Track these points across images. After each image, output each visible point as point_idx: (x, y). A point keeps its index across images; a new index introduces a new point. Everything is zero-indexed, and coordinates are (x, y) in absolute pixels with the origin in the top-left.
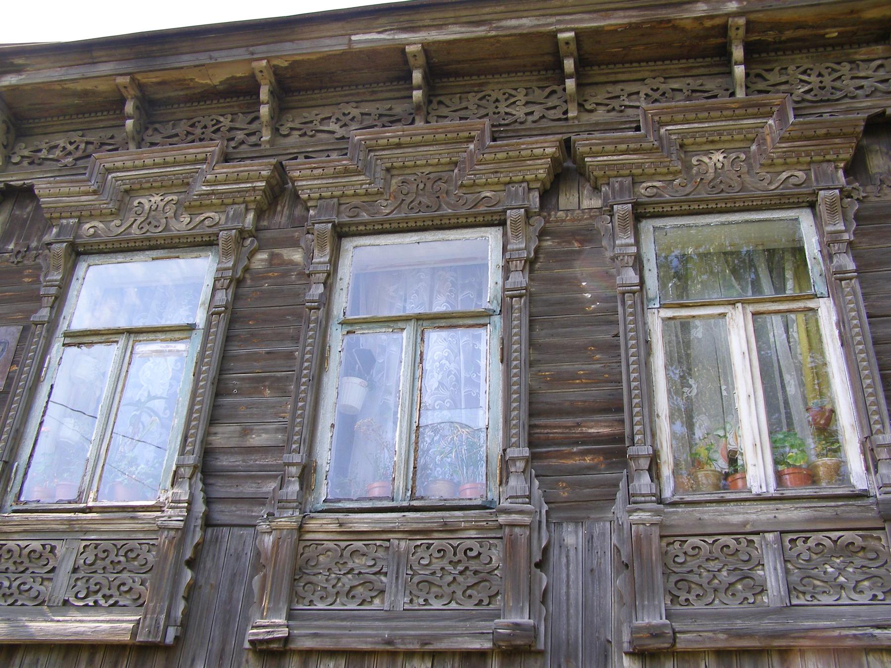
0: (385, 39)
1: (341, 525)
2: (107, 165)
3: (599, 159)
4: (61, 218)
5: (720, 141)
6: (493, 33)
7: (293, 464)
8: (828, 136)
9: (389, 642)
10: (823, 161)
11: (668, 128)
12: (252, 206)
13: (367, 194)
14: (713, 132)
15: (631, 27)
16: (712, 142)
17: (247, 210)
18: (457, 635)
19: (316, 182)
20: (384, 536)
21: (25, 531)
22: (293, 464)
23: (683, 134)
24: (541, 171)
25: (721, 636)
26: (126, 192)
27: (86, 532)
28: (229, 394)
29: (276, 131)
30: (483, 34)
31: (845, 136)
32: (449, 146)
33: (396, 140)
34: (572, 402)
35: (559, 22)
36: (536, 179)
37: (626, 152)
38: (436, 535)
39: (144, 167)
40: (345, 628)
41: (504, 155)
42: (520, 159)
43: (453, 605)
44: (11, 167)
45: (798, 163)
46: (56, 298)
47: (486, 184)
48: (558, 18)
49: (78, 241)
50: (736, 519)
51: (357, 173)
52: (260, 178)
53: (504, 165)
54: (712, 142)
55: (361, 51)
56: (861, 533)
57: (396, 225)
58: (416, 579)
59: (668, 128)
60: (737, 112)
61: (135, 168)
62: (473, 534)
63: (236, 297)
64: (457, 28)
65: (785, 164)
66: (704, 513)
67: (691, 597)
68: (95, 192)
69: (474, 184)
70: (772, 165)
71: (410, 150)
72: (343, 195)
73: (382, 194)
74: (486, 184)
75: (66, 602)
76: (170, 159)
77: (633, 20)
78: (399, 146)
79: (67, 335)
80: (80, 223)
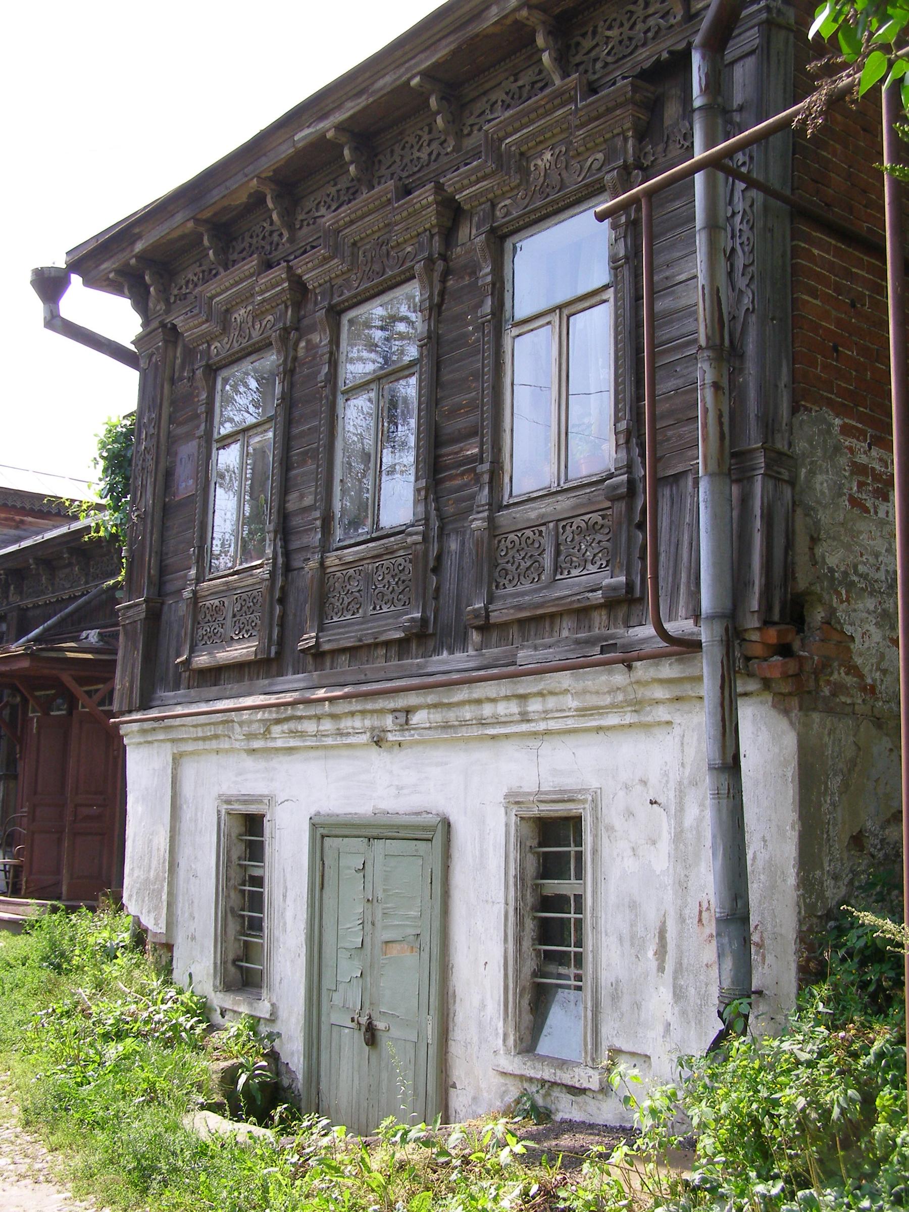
0: (311, 133)
1: (340, 559)
2: (209, 295)
3: (464, 193)
4: (198, 345)
5: (545, 140)
6: (371, 100)
7: (316, 519)
8: (609, 111)
9: (360, 640)
10: (614, 137)
11: (507, 141)
12: (289, 303)
13: (343, 273)
14: (542, 132)
15: (454, 53)
16: (541, 142)
17: (287, 307)
18: (389, 630)
19: (313, 273)
20: (361, 563)
21: (212, 594)
22: (316, 519)
23: (517, 143)
24: (430, 218)
25: (512, 611)
26: (227, 311)
27: (235, 589)
28: (294, 468)
29: (291, 228)
30: (364, 103)
31: (618, 106)
32: (381, 211)
33: (347, 219)
34: (459, 430)
35: (408, 70)
36: (433, 226)
37: (478, 181)
38: (385, 557)
39: (227, 289)
40: (339, 634)
41: (405, 214)
42: (416, 213)
43: (393, 608)
44: (173, 306)
45: (597, 145)
46: (207, 413)
47: (405, 241)
48: (407, 65)
49: (211, 362)
50: (533, 515)
51: (332, 258)
52: (283, 281)
53: (410, 221)
54: (541, 142)
55: (304, 148)
56: (600, 513)
57: (376, 290)
58: (377, 591)
59: (507, 141)
60: (547, 107)
61: (224, 291)
62: (401, 553)
63: (292, 385)
64: (349, 104)
65: (587, 149)
66: (516, 512)
67: (506, 582)
68: (207, 321)
69: (398, 244)
70: (579, 154)
71: (360, 223)
72: (331, 279)
73: (352, 270)
74: (405, 241)
75: (232, 638)
76: (237, 279)
77: (452, 47)
78: (352, 222)
79: (218, 441)
80: (209, 346)
